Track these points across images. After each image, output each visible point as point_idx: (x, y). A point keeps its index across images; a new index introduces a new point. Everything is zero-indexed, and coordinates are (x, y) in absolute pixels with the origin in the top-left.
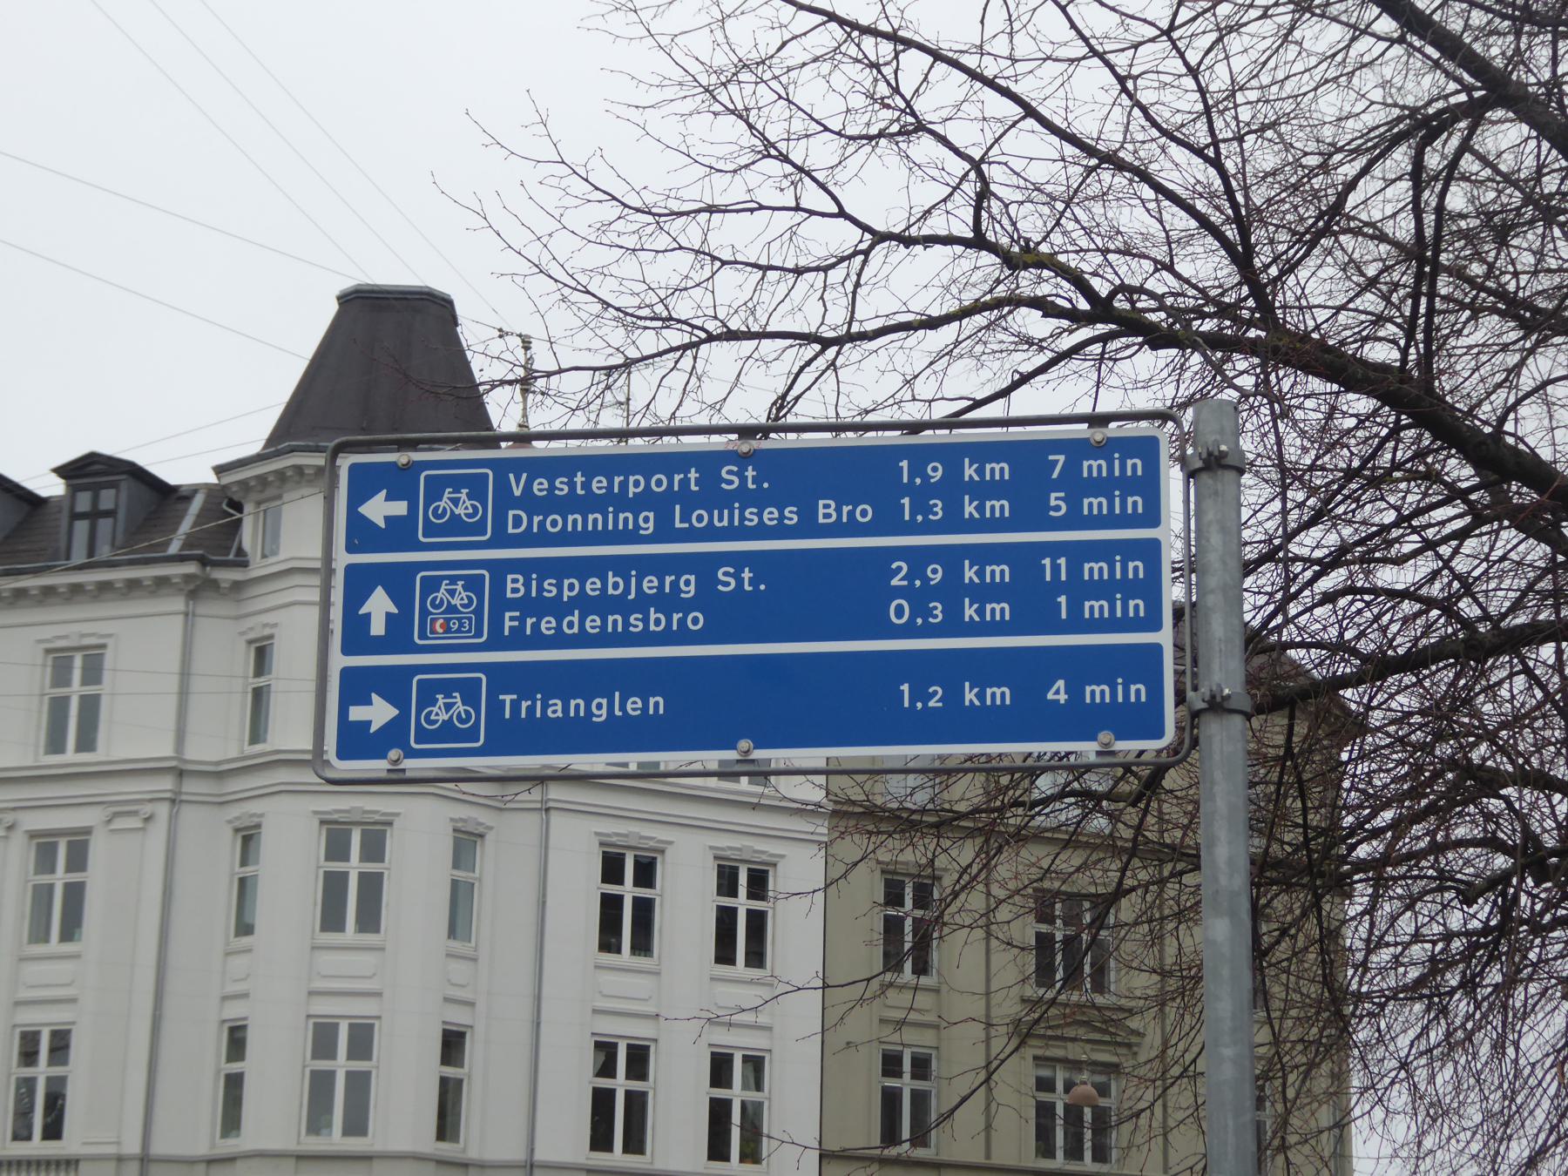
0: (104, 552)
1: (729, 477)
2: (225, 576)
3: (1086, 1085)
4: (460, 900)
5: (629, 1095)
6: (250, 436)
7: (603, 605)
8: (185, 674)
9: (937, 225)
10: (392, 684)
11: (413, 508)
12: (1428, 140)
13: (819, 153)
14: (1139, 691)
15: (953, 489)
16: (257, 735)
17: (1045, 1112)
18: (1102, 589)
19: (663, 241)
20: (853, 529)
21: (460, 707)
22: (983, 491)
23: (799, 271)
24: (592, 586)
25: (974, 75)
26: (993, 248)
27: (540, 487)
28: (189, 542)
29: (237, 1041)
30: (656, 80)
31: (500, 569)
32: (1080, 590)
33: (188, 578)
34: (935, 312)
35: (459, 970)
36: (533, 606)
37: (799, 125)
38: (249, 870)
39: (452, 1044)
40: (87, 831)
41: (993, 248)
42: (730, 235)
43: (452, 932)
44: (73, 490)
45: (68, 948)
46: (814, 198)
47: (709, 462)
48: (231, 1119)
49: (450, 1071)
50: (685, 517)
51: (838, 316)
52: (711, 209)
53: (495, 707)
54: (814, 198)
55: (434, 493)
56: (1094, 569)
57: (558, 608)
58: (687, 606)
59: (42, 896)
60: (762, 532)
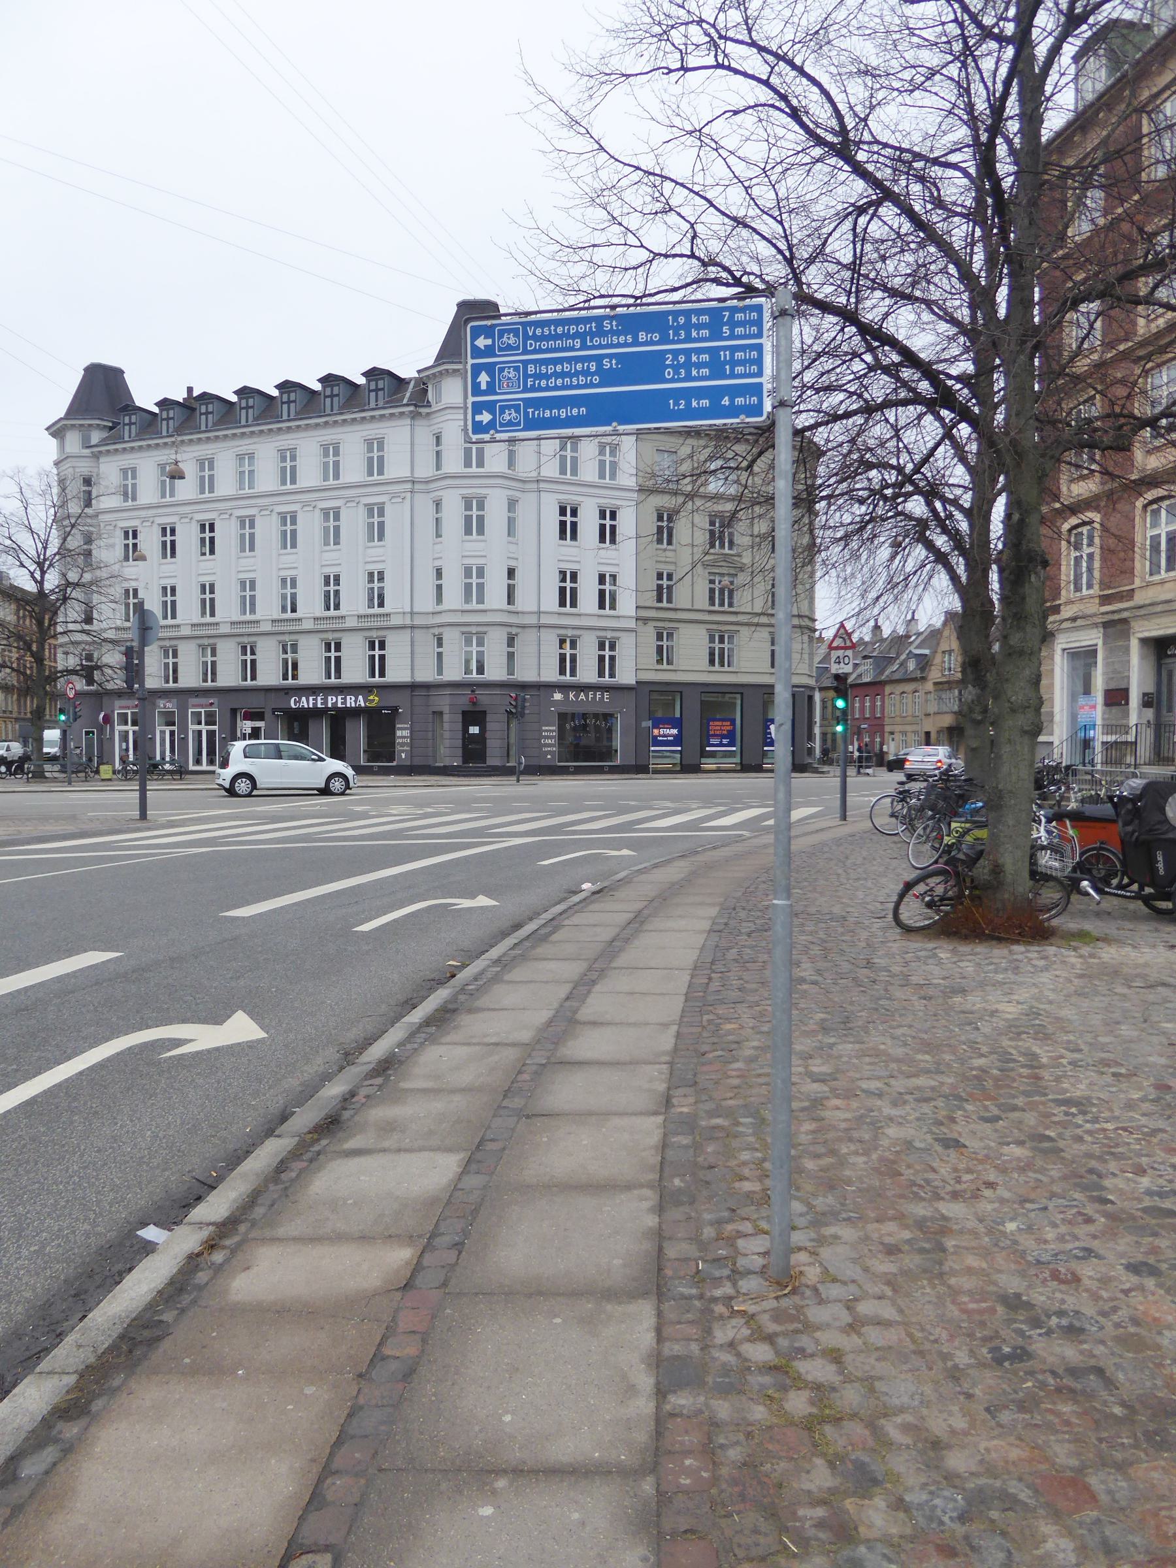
0: (381, 404)
1: (607, 325)
2: (424, 410)
3: (726, 581)
4: (511, 522)
5: (571, 588)
6: (428, 358)
7: (563, 375)
8: (412, 444)
9: (676, 251)
10: (490, 407)
11: (494, 342)
12: (859, 215)
13: (633, 221)
14: (755, 400)
15: (688, 326)
16: (438, 467)
17: (712, 591)
18: (742, 363)
19: (577, 258)
20: (652, 343)
21: (514, 414)
22: (699, 327)
23: (626, 269)
24: (559, 368)
25: (691, 191)
26: (699, 259)
27: (539, 332)
28: (410, 399)
29: (439, 573)
30: (571, 195)
31: (526, 363)
32: (734, 363)
33: (411, 412)
34: (677, 285)
35: (512, 548)
36: (538, 376)
37: (626, 209)
38: (439, 515)
39: (511, 573)
40: (384, 503)
41: (699, 259)
42: (601, 255)
43: (509, 535)
44: (369, 381)
45: (381, 543)
46: (632, 240)
47: (599, 319)
48: (439, 599)
49: (511, 582)
50: (591, 341)
51: (641, 287)
52: (594, 246)
53: (526, 414)
54: (632, 240)
55: (501, 336)
56: (739, 355)
57: (547, 377)
58: (593, 374)
59: (371, 526)
60: (619, 345)
